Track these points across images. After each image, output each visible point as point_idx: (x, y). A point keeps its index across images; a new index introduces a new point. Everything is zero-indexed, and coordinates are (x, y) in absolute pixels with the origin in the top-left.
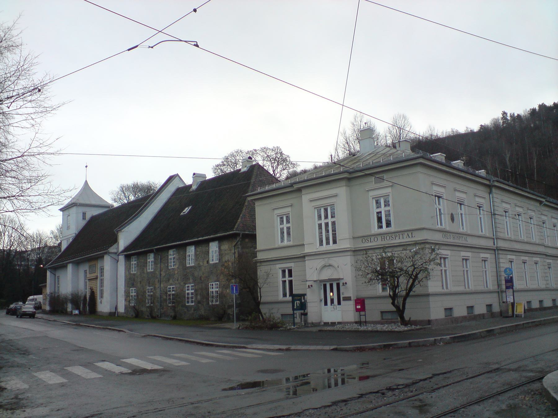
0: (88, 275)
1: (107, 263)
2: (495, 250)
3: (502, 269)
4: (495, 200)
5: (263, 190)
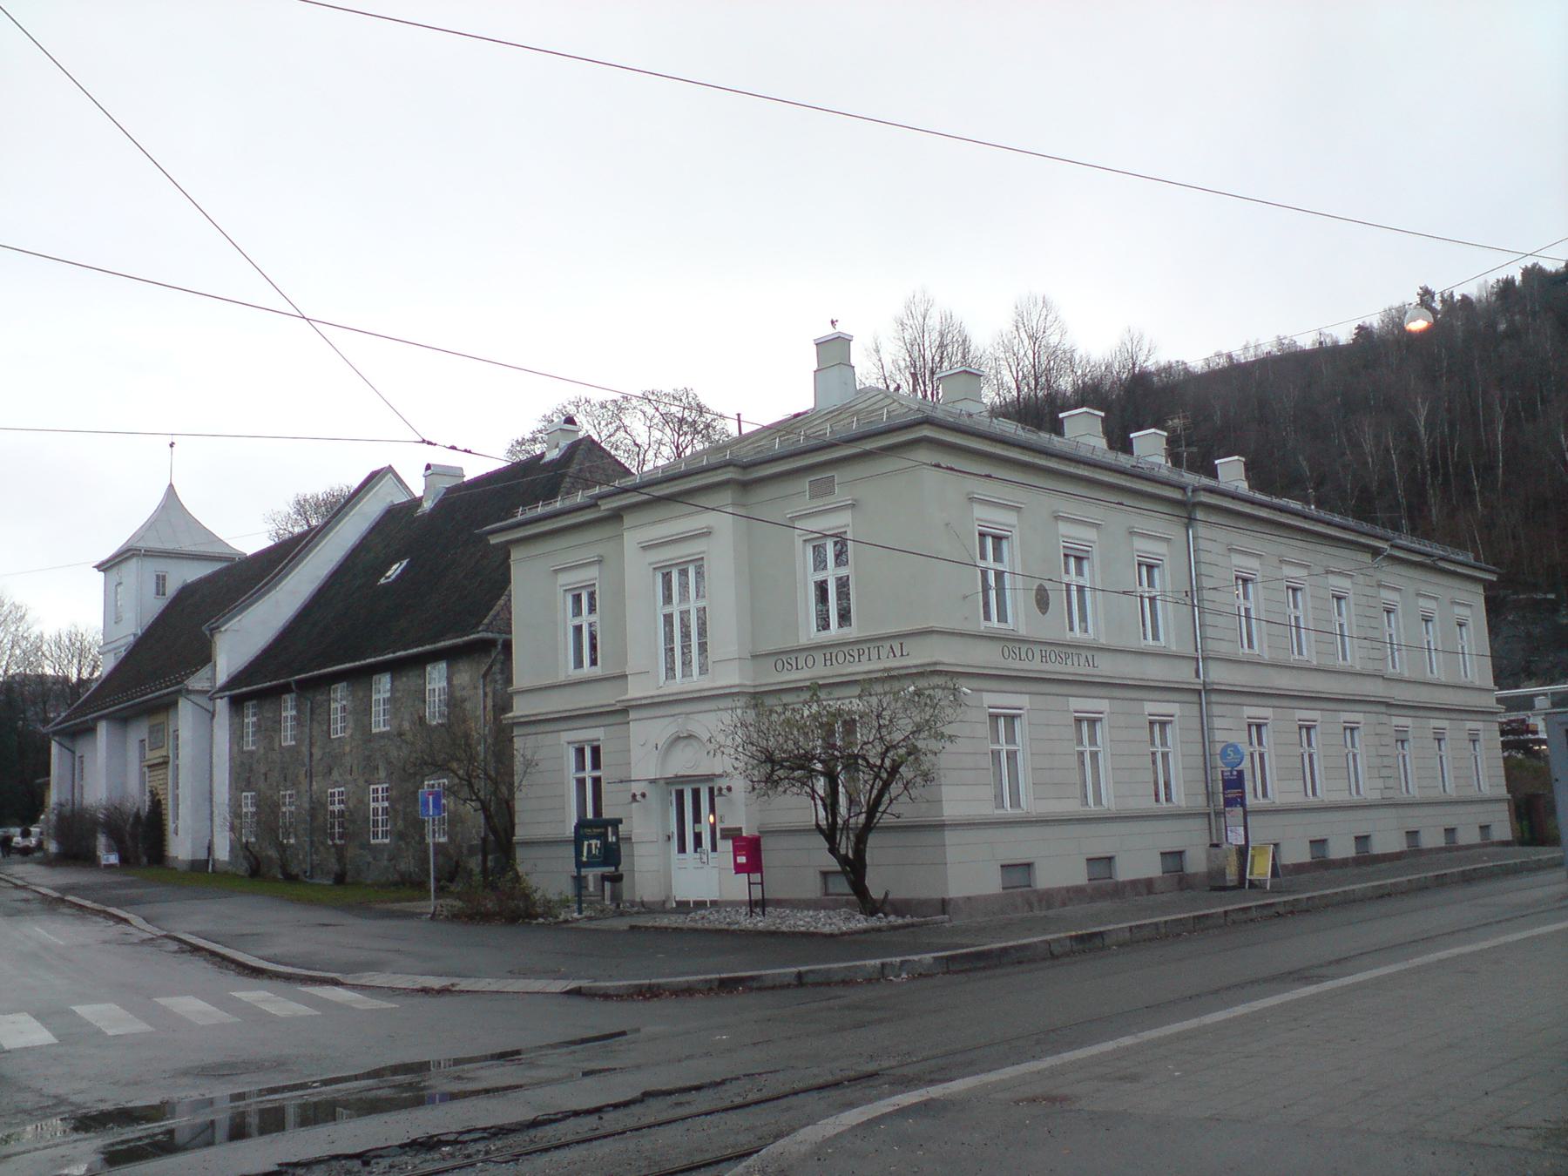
0: (149, 755)
1: (186, 718)
2: (1199, 692)
3: (1218, 748)
4: (1203, 544)
5: (530, 514)
